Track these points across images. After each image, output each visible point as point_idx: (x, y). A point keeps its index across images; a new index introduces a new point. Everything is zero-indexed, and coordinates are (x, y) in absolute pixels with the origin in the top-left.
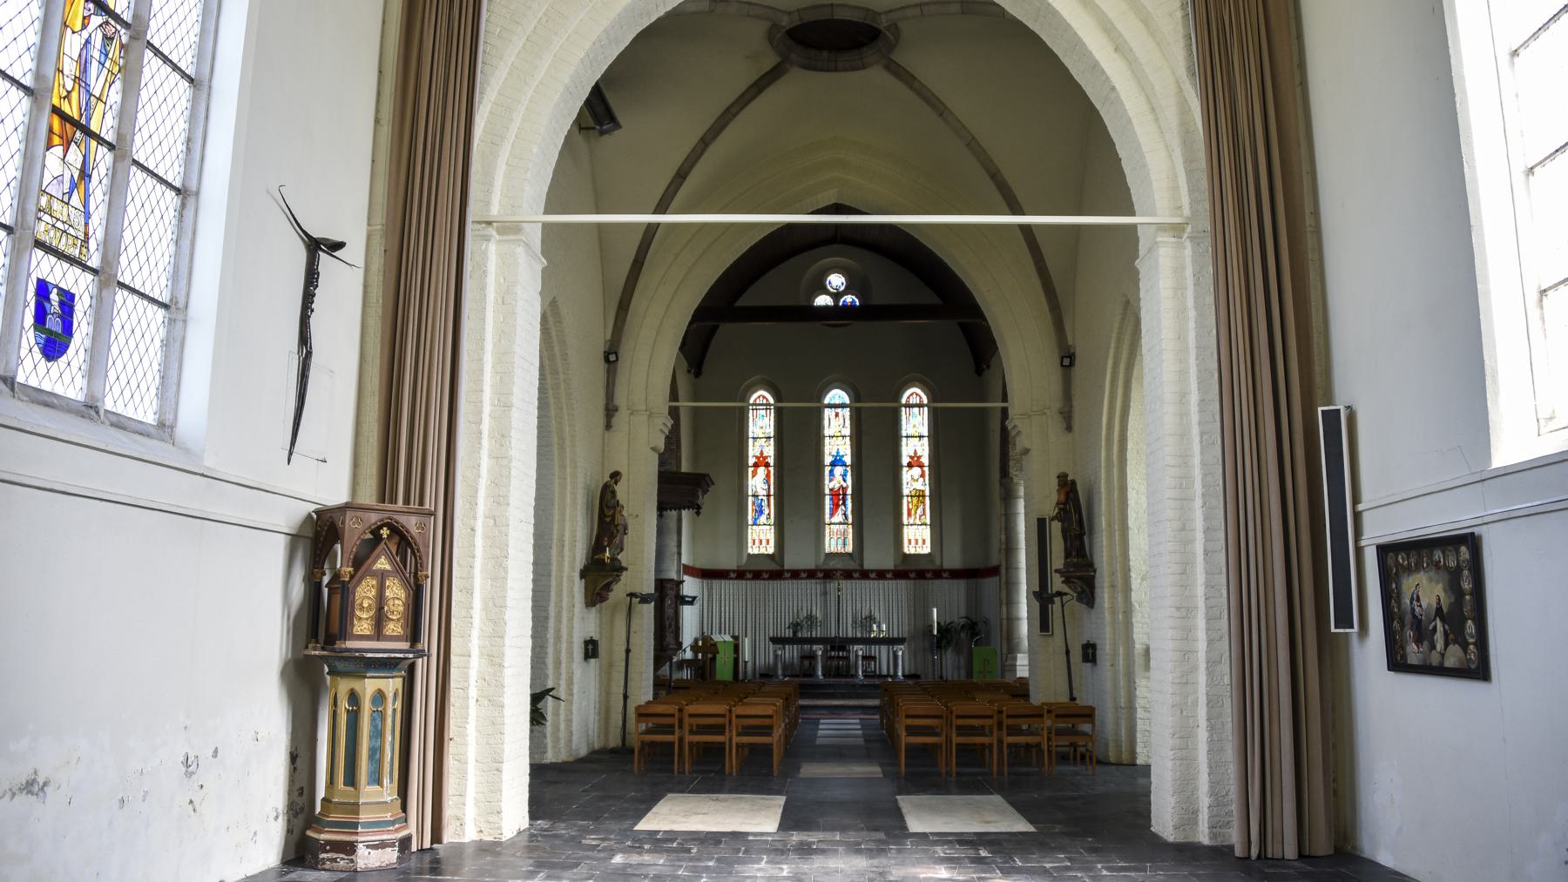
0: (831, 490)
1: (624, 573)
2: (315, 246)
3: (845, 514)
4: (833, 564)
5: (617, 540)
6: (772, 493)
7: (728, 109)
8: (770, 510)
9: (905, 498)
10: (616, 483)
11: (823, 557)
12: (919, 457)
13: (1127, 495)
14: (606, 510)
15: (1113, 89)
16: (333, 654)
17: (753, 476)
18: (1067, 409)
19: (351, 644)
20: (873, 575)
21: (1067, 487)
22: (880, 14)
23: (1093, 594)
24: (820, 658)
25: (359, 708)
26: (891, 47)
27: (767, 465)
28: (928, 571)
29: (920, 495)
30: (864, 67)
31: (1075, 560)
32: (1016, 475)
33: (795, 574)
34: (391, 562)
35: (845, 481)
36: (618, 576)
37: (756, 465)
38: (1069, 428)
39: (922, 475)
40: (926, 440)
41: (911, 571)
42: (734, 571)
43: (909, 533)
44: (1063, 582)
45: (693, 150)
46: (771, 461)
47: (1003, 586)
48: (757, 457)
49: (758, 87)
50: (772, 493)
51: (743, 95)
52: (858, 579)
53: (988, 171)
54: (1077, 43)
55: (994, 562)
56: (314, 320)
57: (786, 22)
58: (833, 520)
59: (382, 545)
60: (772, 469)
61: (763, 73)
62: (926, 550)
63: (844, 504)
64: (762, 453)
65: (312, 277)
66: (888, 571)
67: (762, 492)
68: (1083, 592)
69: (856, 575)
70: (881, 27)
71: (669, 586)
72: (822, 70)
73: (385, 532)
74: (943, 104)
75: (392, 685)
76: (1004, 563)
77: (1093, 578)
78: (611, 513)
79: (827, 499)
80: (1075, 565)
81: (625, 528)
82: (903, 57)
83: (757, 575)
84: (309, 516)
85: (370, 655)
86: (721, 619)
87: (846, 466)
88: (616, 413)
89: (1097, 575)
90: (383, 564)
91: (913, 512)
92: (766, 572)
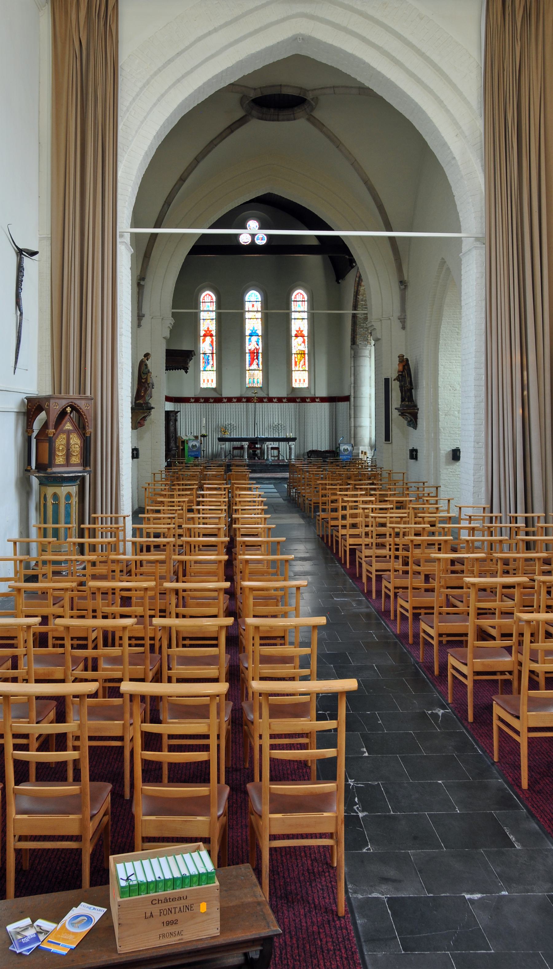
0: (249, 350)
1: (153, 410)
2: (20, 252)
3: (258, 364)
4: (250, 394)
5: (149, 392)
6: (214, 352)
7: (212, 141)
8: (213, 362)
9: (293, 355)
10: (147, 360)
11: (245, 390)
12: (302, 331)
13: (438, 368)
14: (143, 375)
15: (454, 158)
16: (46, 475)
17: (203, 342)
18: (403, 317)
19: (55, 470)
20: (275, 400)
21: (404, 363)
22: (308, 91)
23: (416, 422)
24: (246, 449)
25: (59, 502)
26: (313, 109)
27: (211, 336)
28: (307, 398)
29: (303, 353)
30: (295, 119)
31: (407, 403)
32: (360, 344)
33: (230, 400)
34: (72, 426)
35: (257, 345)
36: (150, 412)
37: (205, 336)
38: (404, 328)
39: (304, 342)
40: (306, 321)
41: (298, 398)
42: (193, 398)
43: (295, 375)
44: (399, 415)
45: (190, 165)
46: (214, 333)
47: (352, 407)
48: (205, 331)
49: (231, 128)
50: (214, 352)
51: (221, 133)
52: (266, 402)
53: (363, 180)
54: (435, 131)
55: (346, 394)
56: (23, 295)
57: (253, 95)
58: (252, 368)
59: (67, 417)
60: (214, 338)
61: (234, 121)
62: (306, 385)
63: (257, 358)
64: (208, 328)
65: (20, 269)
66: (284, 398)
67: (208, 351)
68: (411, 420)
69: (265, 400)
70: (308, 99)
71: (171, 414)
72: (270, 120)
73: (69, 410)
74: (339, 140)
75: (74, 489)
76: (352, 394)
77: (417, 413)
78: (145, 377)
79: (247, 355)
80: (407, 406)
81: (153, 385)
82: (317, 114)
83: (207, 400)
84: (23, 401)
85: (66, 475)
86: (186, 429)
87: (258, 336)
88: (144, 318)
89: (419, 412)
90: (68, 426)
91: (298, 363)
92: (212, 398)
